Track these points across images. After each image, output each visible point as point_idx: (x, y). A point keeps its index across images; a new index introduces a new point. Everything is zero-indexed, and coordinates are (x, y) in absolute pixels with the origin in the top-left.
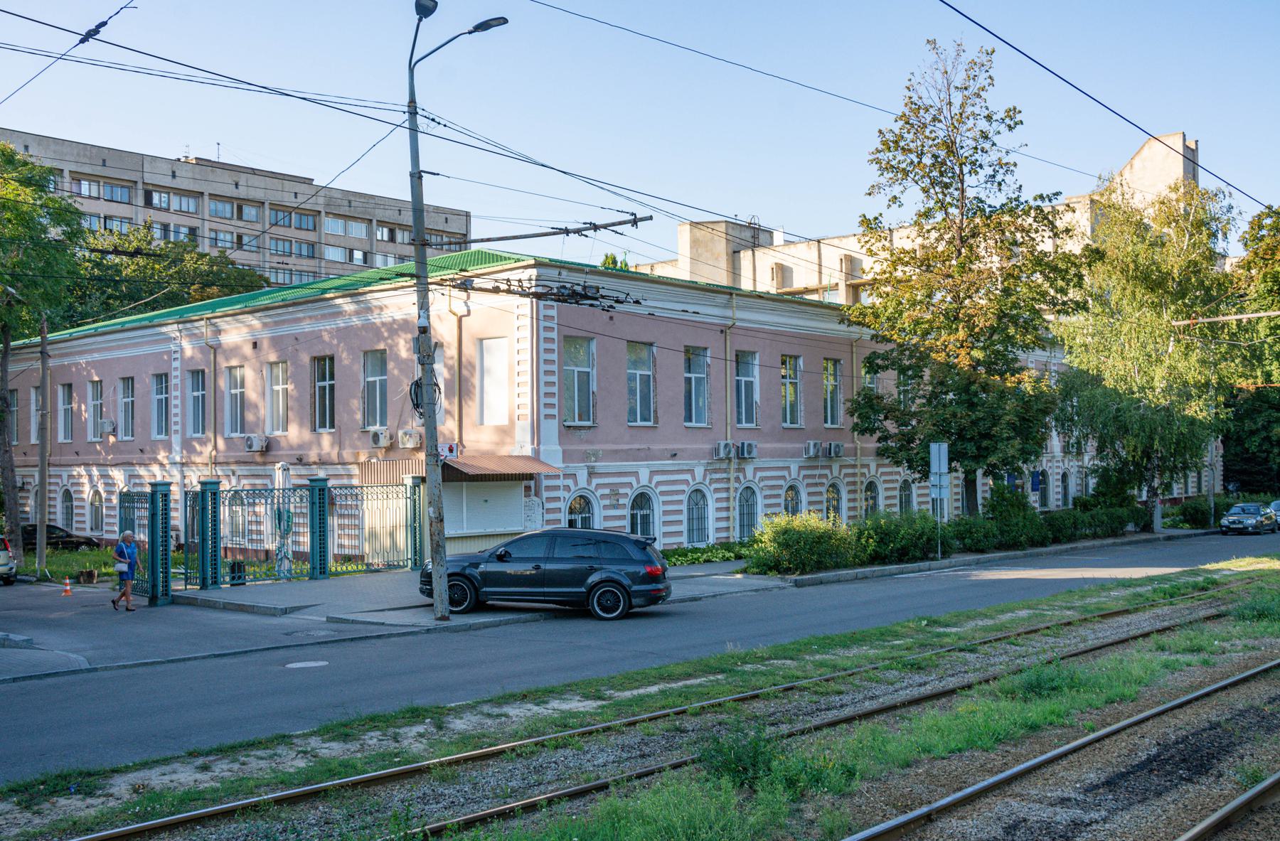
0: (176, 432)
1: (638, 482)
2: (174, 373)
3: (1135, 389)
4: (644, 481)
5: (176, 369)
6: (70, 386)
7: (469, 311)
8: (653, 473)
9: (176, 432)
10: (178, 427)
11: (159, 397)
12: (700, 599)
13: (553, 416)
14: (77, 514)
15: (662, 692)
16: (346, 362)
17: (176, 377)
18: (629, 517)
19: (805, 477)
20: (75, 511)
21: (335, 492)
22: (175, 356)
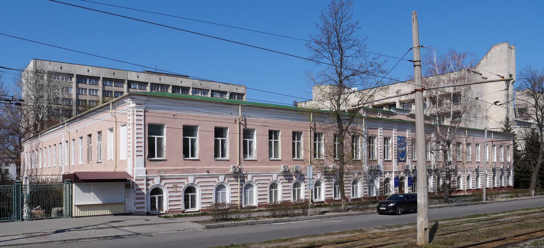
1: (188, 182)
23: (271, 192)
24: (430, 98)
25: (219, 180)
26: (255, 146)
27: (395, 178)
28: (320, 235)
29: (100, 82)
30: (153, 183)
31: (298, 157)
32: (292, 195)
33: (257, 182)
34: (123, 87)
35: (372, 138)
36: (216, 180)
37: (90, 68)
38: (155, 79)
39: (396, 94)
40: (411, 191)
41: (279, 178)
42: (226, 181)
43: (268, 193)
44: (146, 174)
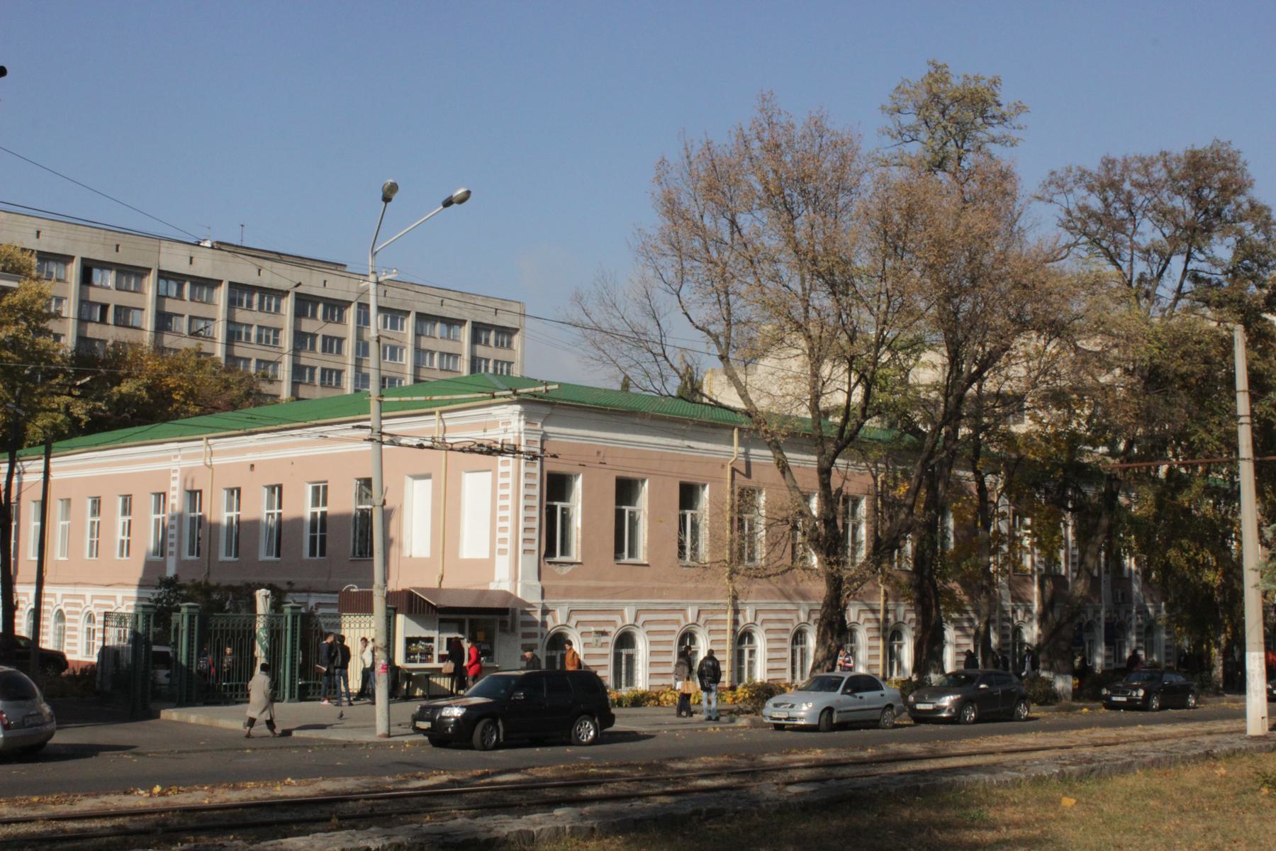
0: (171, 553)
1: (623, 620)
2: (172, 493)
3: (735, 253)
4: (629, 620)
5: (174, 489)
6: (69, 500)
7: (298, 399)
8: (638, 613)
9: (171, 553)
10: (174, 549)
11: (157, 516)
12: (346, 800)
13: (532, 551)
14: (70, 636)
15: (863, 748)
16: (1143, 657)
17: (174, 497)
18: (611, 658)
19: (763, 621)
20: (67, 633)
21: (321, 620)
22: (174, 475)
23: (617, 658)
24: (360, 305)
25: (686, 618)
26: (577, 522)
27: (1106, 624)
28: (505, 789)
29: (150, 284)
30: (554, 620)
31: (563, 553)
32: (788, 665)
33: (581, 629)
34: (210, 302)
35: (754, 491)
36: (679, 616)
37: (44, 225)
38: (245, 272)
39: (446, 301)
40: (1112, 661)
41: (863, 616)
42: (573, 623)
43: (788, 655)
44: (543, 597)
